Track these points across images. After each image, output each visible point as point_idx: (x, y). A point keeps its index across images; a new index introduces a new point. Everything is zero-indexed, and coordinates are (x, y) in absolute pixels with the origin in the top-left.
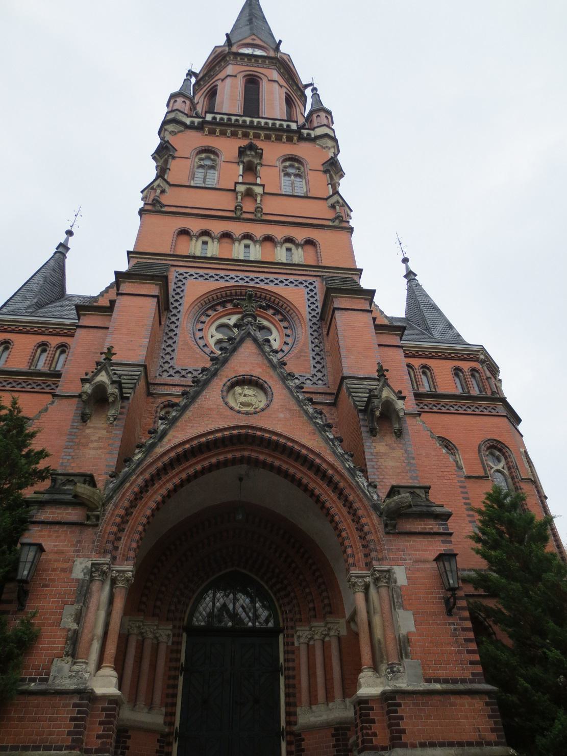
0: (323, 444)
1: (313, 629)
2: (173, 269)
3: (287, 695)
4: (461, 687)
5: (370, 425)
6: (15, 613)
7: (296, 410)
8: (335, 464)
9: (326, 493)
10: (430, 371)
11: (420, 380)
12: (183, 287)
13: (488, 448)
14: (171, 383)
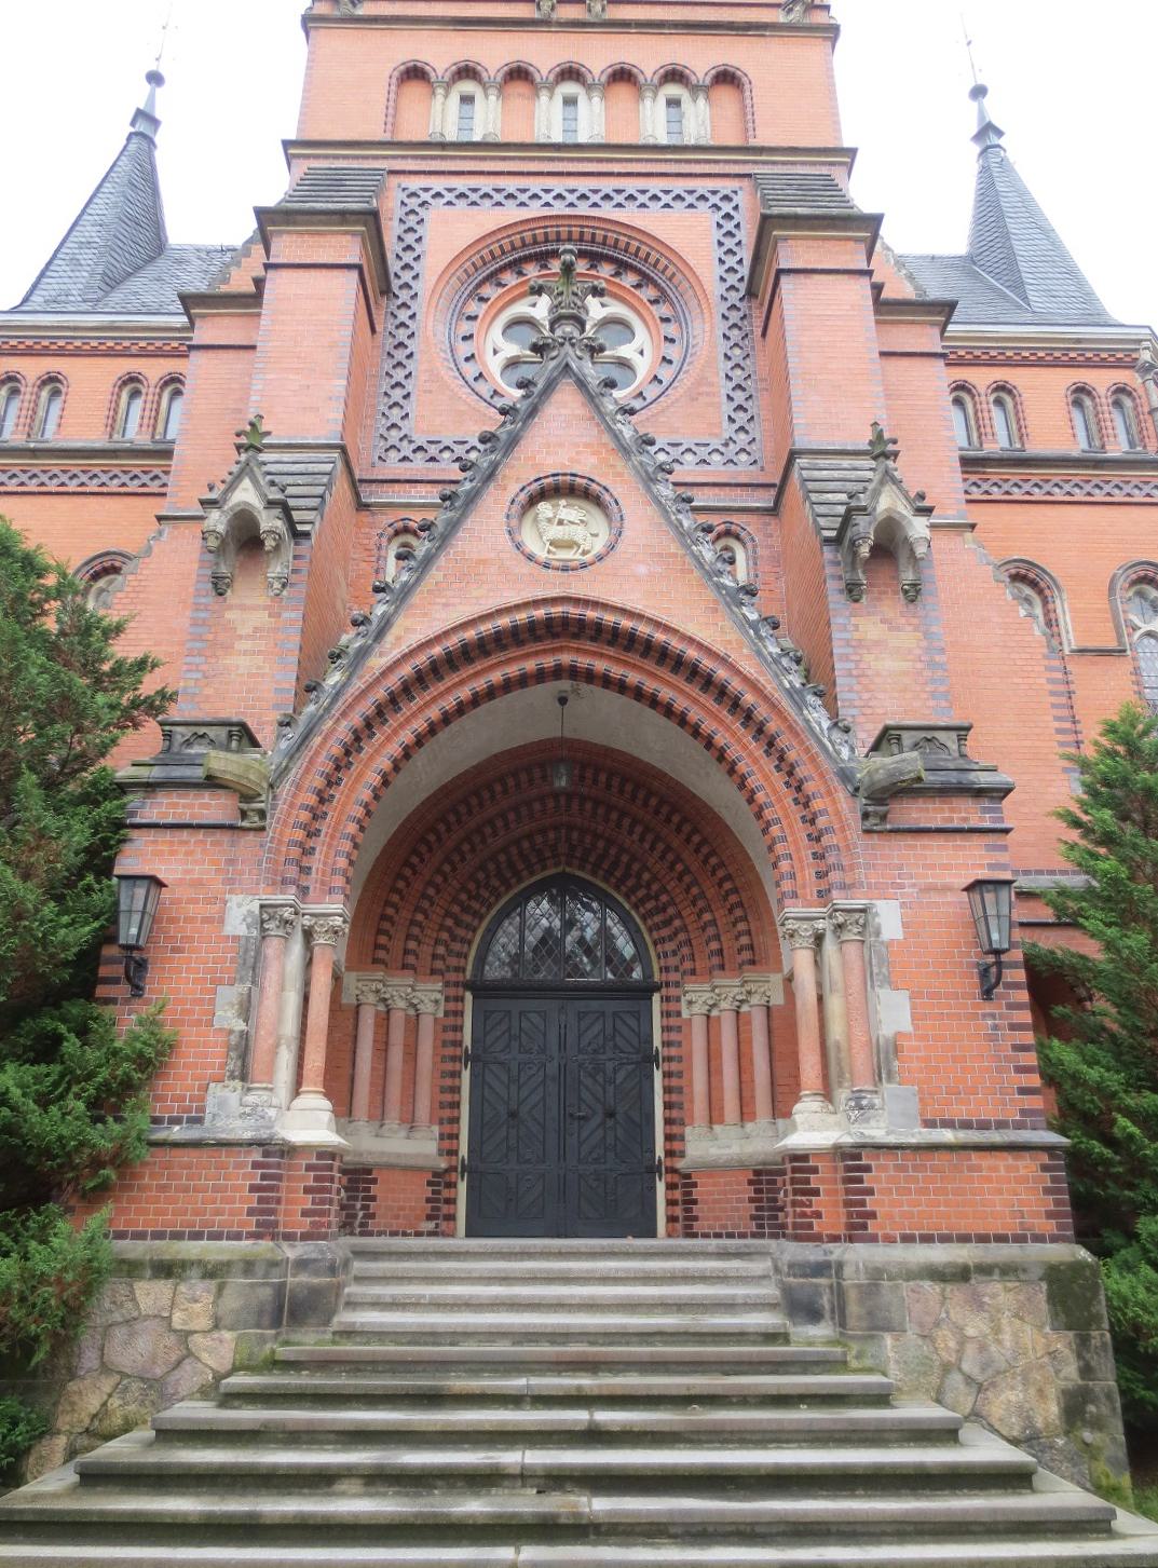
0: (734, 635)
1: (717, 991)
2: (394, 181)
3: (668, 1106)
4: (995, 1137)
5: (848, 575)
6: (126, 1001)
7: (675, 555)
8: (761, 679)
9: (739, 741)
10: (1014, 397)
11: (987, 422)
12: (420, 230)
13: (1134, 583)
14: (408, 478)
